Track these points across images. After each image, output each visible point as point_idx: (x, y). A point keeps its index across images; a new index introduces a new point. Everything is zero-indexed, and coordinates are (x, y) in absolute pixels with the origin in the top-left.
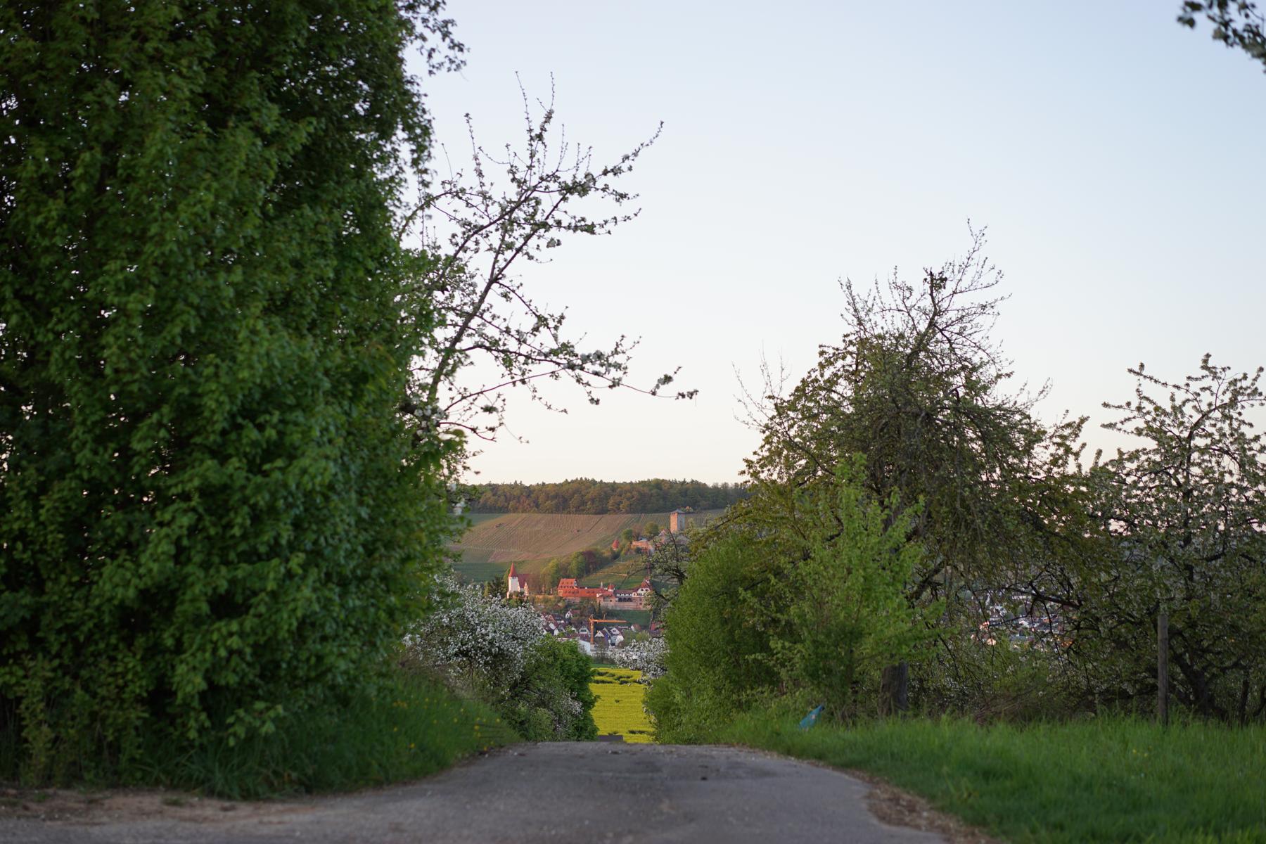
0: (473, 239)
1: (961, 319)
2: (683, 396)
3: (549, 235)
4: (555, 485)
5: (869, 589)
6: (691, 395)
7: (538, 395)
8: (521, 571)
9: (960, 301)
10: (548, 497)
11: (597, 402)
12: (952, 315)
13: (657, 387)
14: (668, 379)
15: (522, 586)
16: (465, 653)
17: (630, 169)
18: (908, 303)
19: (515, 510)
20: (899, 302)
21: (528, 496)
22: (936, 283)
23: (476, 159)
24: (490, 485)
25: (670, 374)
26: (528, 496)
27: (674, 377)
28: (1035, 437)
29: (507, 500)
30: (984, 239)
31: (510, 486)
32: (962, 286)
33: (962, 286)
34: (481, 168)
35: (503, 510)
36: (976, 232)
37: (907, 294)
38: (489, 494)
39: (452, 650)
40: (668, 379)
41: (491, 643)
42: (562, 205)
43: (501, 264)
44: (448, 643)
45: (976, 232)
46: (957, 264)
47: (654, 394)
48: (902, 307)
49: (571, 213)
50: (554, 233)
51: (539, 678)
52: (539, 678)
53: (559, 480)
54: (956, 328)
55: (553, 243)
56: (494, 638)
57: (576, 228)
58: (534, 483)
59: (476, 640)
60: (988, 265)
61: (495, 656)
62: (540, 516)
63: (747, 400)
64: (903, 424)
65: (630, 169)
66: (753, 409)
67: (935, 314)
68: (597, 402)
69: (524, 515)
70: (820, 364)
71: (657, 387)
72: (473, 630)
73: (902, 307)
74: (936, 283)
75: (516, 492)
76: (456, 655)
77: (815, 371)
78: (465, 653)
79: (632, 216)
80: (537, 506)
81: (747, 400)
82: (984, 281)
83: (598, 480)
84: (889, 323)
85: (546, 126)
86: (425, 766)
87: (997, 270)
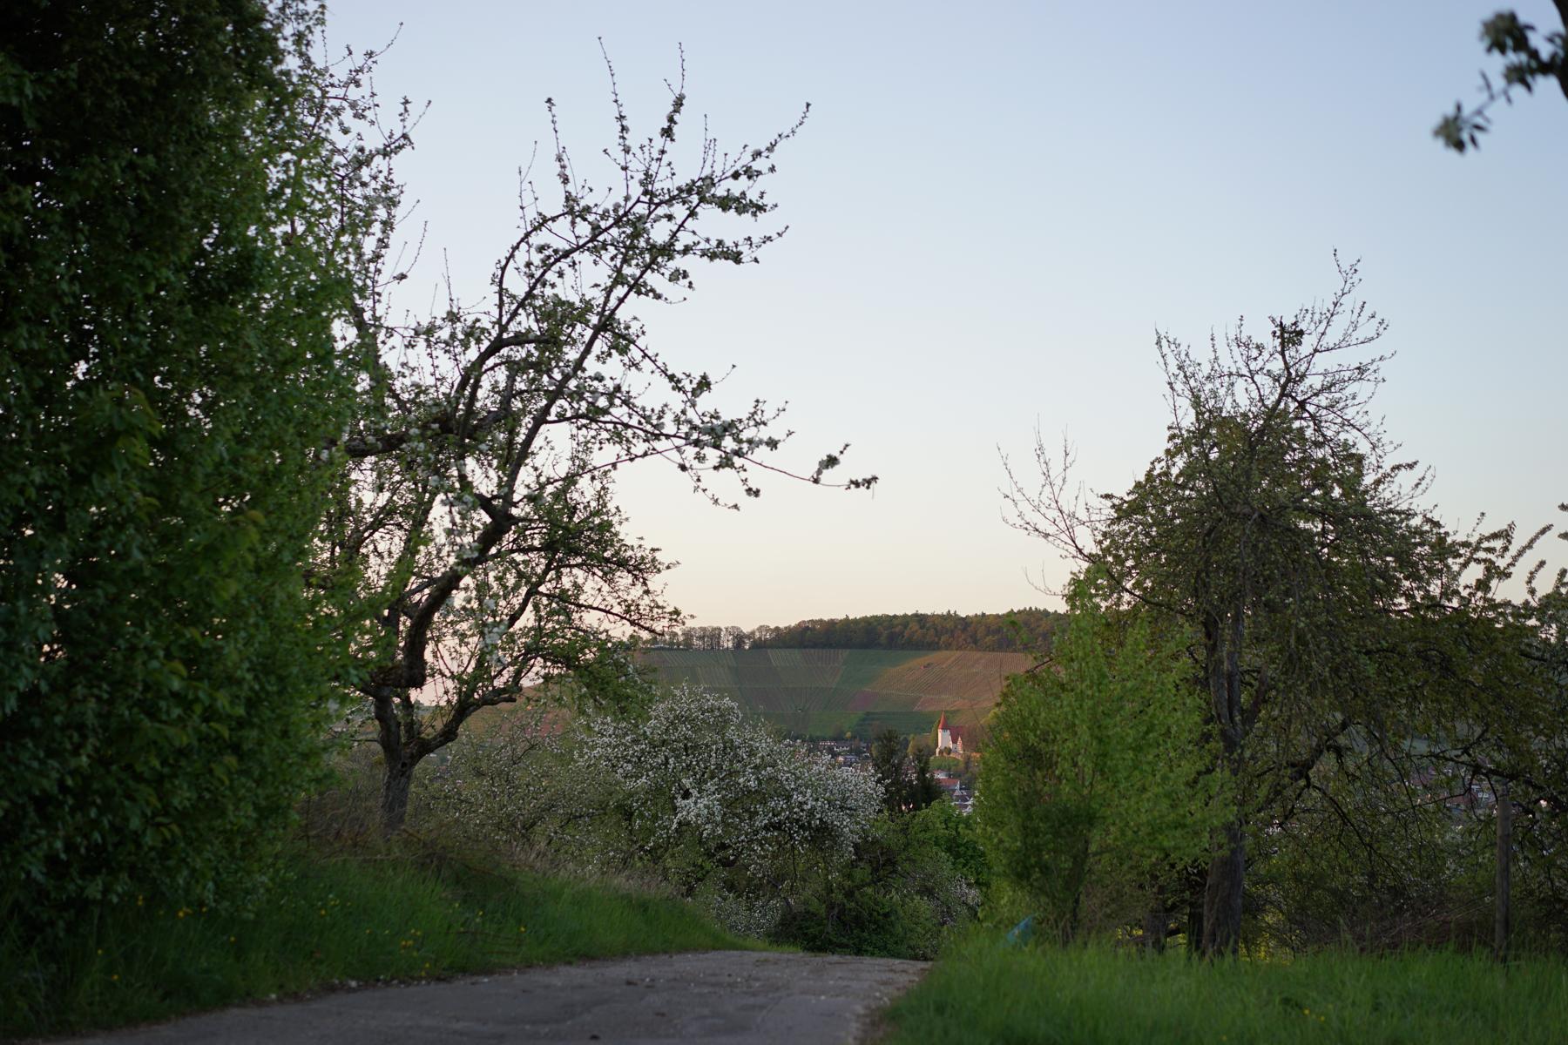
0: (556, 268)
1: (1326, 388)
2: (857, 484)
3: (672, 265)
4: (998, 616)
5: (1105, 755)
6: (868, 482)
7: (702, 485)
8: (955, 722)
9: (1322, 362)
10: (989, 632)
11: (757, 493)
12: (1315, 381)
13: (819, 472)
14: (831, 461)
15: (955, 741)
16: (777, 827)
17: (772, 169)
18: (1253, 365)
19: (948, 646)
20: (1241, 364)
21: (964, 630)
22: (1289, 336)
23: (560, 159)
24: (916, 615)
25: (836, 454)
26: (964, 630)
27: (841, 458)
28: (1444, 549)
29: (938, 634)
30: (1356, 277)
31: (942, 616)
32: (1330, 340)
33: (1330, 340)
34: (568, 172)
35: (933, 646)
36: (1345, 267)
37: (1255, 353)
38: (914, 626)
39: (761, 821)
40: (831, 461)
41: (811, 813)
42: (690, 224)
43: (613, 303)
44: (757, 813)
45: (1345, 267)
46: (1317, 311)
47: (816, 481)
48: (1245, 371)
49: (703, 234)
50: (679, 262)
51: (908, 859)
52: (908, 859)
53: (1002, 610)
54: (1323, 400)
55: (677, 275)
56: (814, 808)
57: (713, 256)
58: (971, 614)
59: (790, 809)
60: (1367, 312)
61: (818, 830)
62: (979, 654)
63: (1018, 496)
64: (1256, 534)
65: (772, 169)
66: (1025, 507)
67: (1289, 380)
68: (757, 493)
69: (958, 653)
70: (1168, 451)
71: (819, 472)
72: (789, 798)
73: (1245, 371)
74: (1289, 336)
75: (949, 625)
76: (766, 828)
77: (1159, 460)
78: (777, 827)
79: (774, 236)
80: (975, 642)
81: (1018, 496)
82: (1361, 334)
83: (1051, 610)
84: (1241, 399)
85: (677, 117)
86: (375, 970)
87: (1378, 319)
